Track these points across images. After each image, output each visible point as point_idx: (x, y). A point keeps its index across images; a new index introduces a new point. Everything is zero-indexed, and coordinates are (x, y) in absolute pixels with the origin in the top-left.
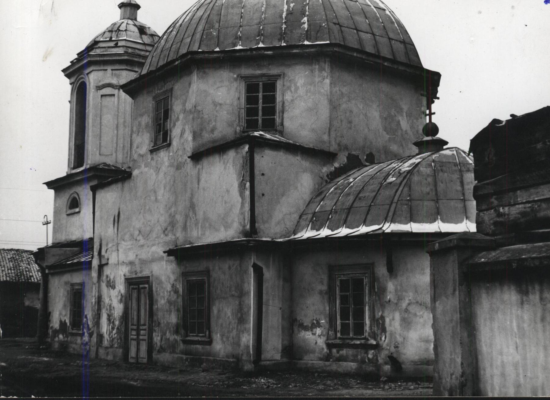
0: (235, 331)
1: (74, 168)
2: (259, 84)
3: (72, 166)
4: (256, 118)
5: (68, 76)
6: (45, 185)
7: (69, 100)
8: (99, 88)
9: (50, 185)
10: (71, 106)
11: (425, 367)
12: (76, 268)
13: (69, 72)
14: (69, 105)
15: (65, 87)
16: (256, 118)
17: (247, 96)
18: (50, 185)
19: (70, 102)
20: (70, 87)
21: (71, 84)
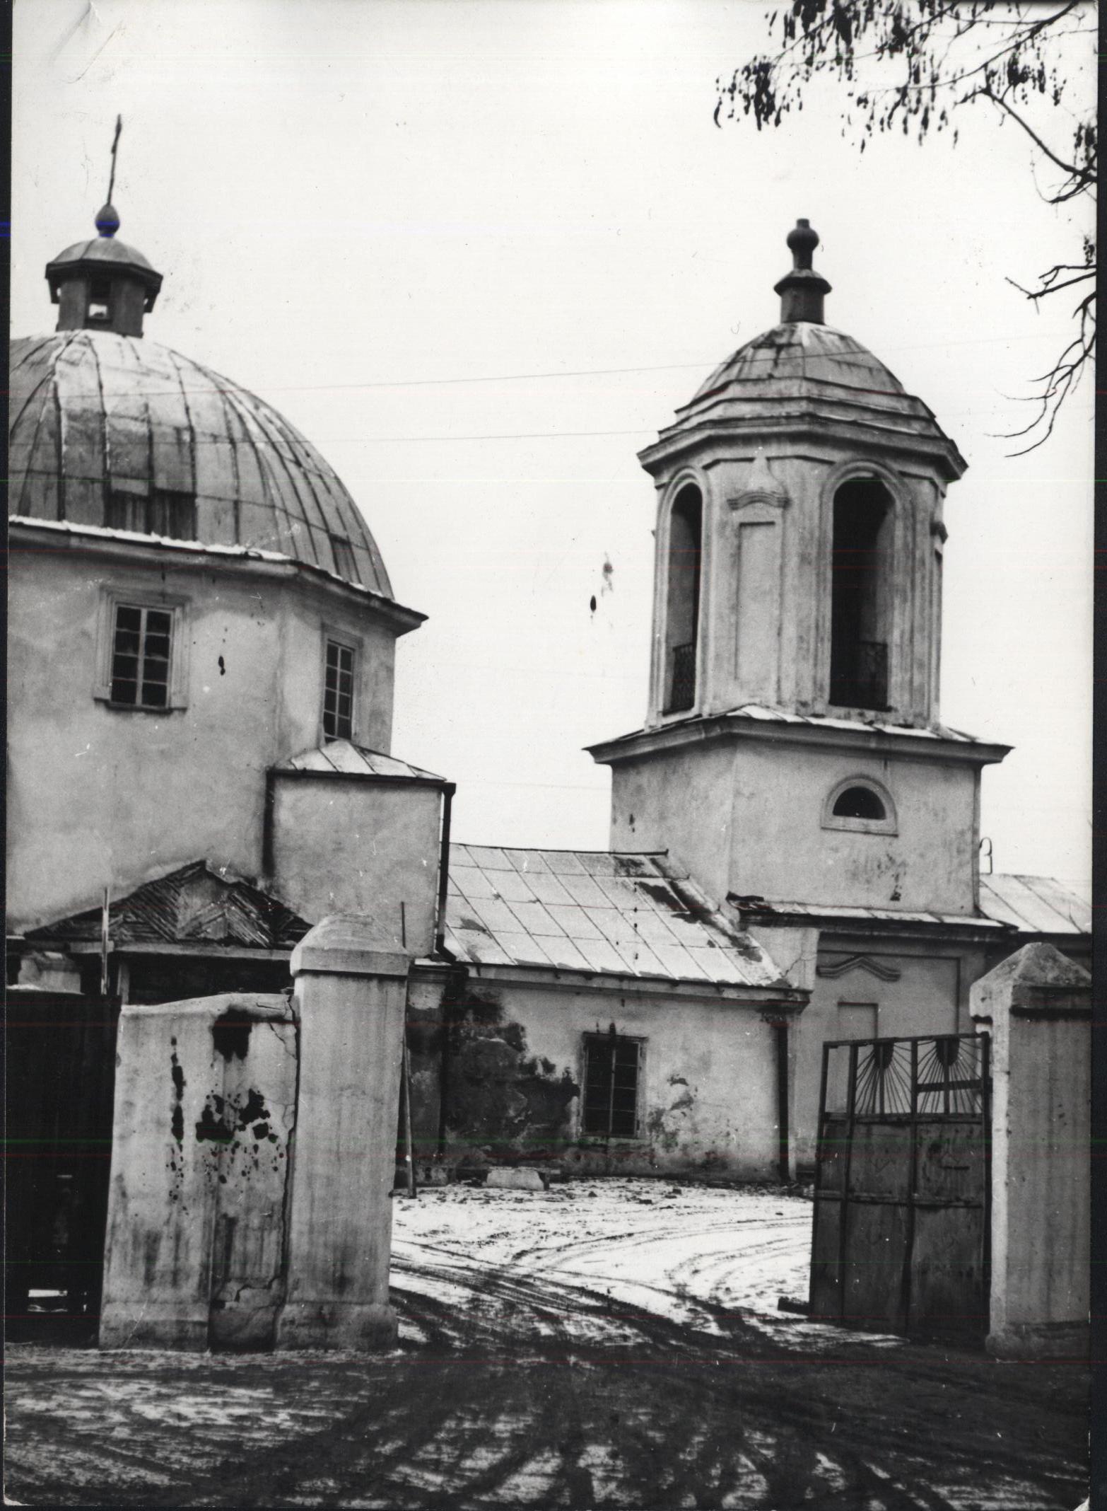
0: (134, 919)
1: (666, 713)
2: (144, 702)
3: (661, 708)
4: (153, 634)
5: (653, 469)
6: (587, 753)
7: (653, 527)
8: (733, 504)
9: (597, 751)
10: (657, 545)
11: (164, 1391)
12: (935, 594)
13: (657, 464)
14: (652, 540)
15: (642, 506)
16: (153, 634)
17: (118, 634)
18: (597, 751)
19: (653, 533)
20: (654, 496)
21: (658, 488)
